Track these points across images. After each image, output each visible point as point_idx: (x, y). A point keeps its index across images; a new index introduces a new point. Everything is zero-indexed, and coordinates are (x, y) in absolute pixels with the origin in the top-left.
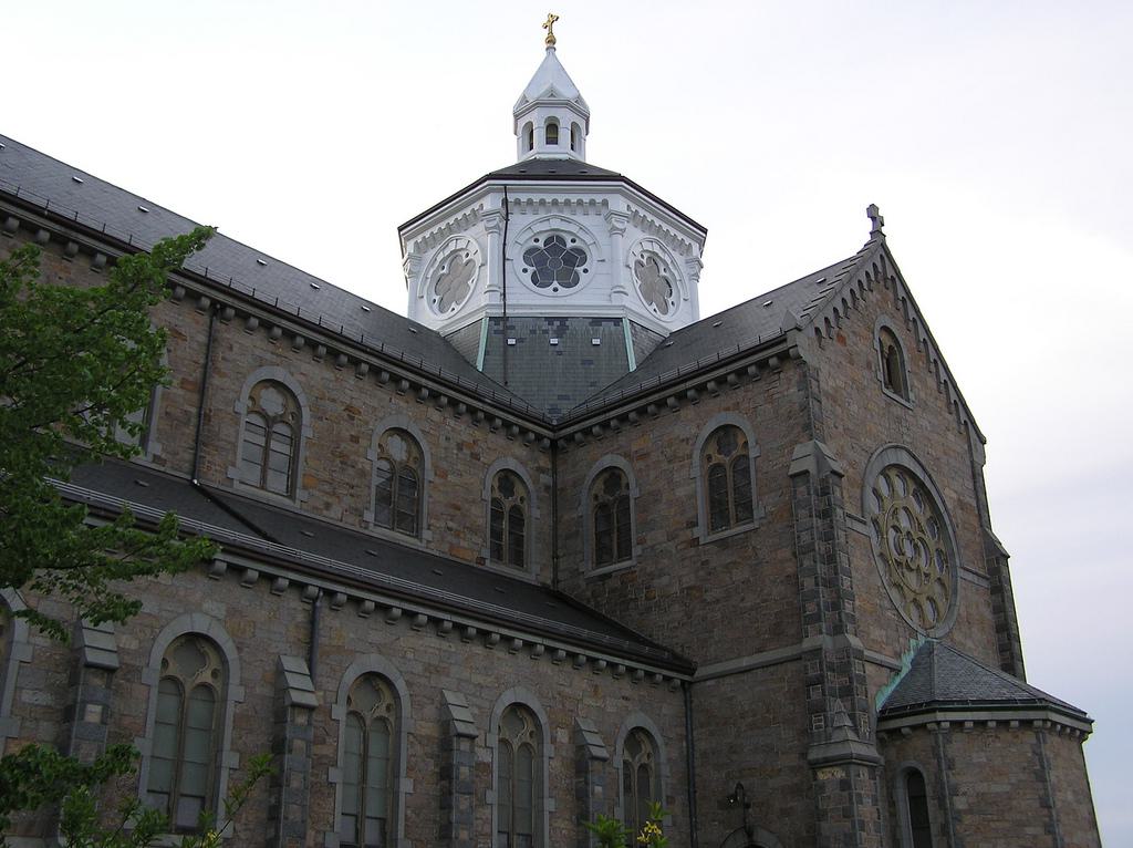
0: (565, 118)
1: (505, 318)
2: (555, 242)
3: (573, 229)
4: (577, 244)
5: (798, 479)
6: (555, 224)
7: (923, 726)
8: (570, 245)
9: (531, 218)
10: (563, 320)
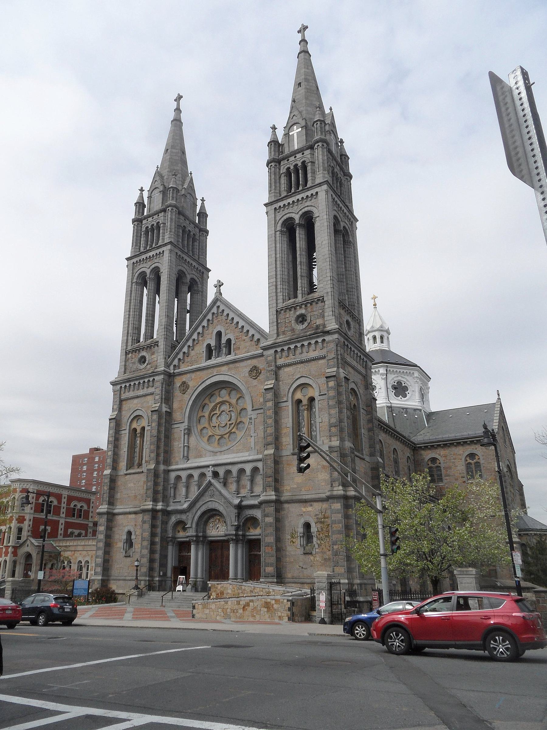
0: (385, 334)
1: (391, 407)
2: (399, 383)
3: (405, 381)
4: (406, 385)
5: (154, 413)
6: (400, 378)
7: (527, 534)
8: (403, 385)
9: (393, 376)
10: (406, 409)
